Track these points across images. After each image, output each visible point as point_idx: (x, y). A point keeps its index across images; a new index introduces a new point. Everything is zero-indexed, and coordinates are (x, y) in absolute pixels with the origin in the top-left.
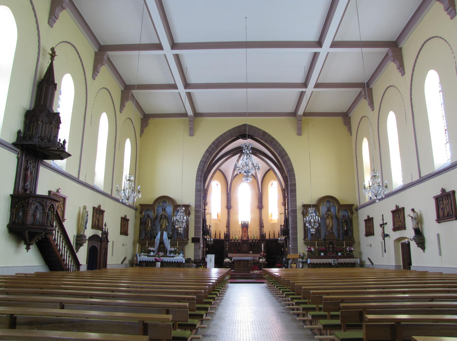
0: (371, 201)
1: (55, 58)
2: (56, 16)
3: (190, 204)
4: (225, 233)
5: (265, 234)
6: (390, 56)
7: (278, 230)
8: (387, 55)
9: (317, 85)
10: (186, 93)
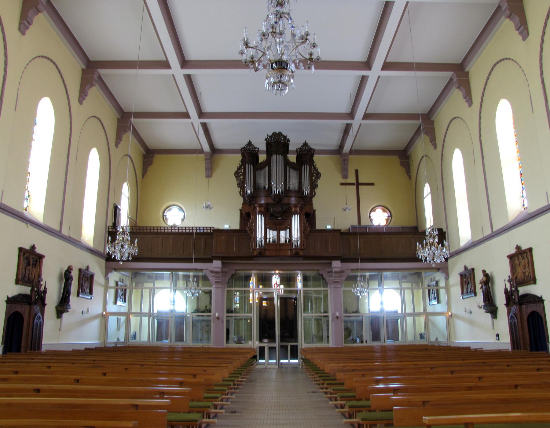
2: (30, 21)
6: (503, 9)
8: (451, 80)
9: (367, 116)
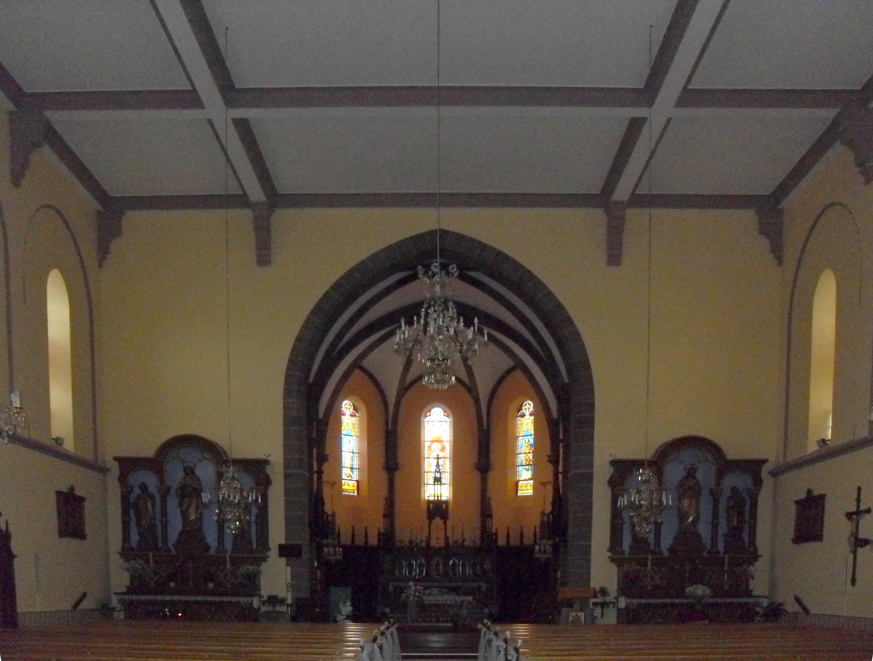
0: (824, 450)
1: (436, 464)
3: (269, 459)
4: (382, 531)
5: (496, 534)
7: (533, 522)
10: (234, 121)
